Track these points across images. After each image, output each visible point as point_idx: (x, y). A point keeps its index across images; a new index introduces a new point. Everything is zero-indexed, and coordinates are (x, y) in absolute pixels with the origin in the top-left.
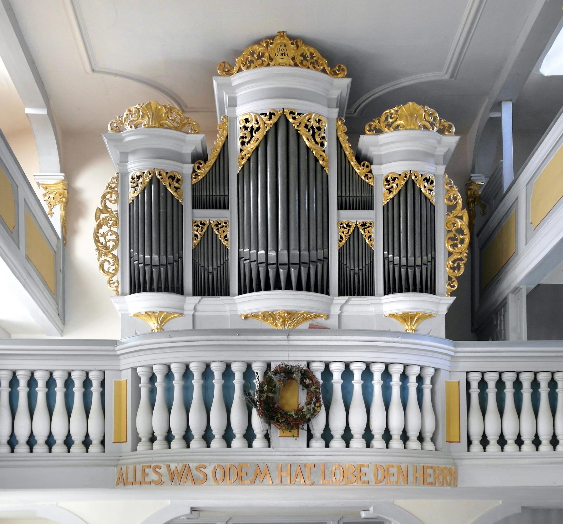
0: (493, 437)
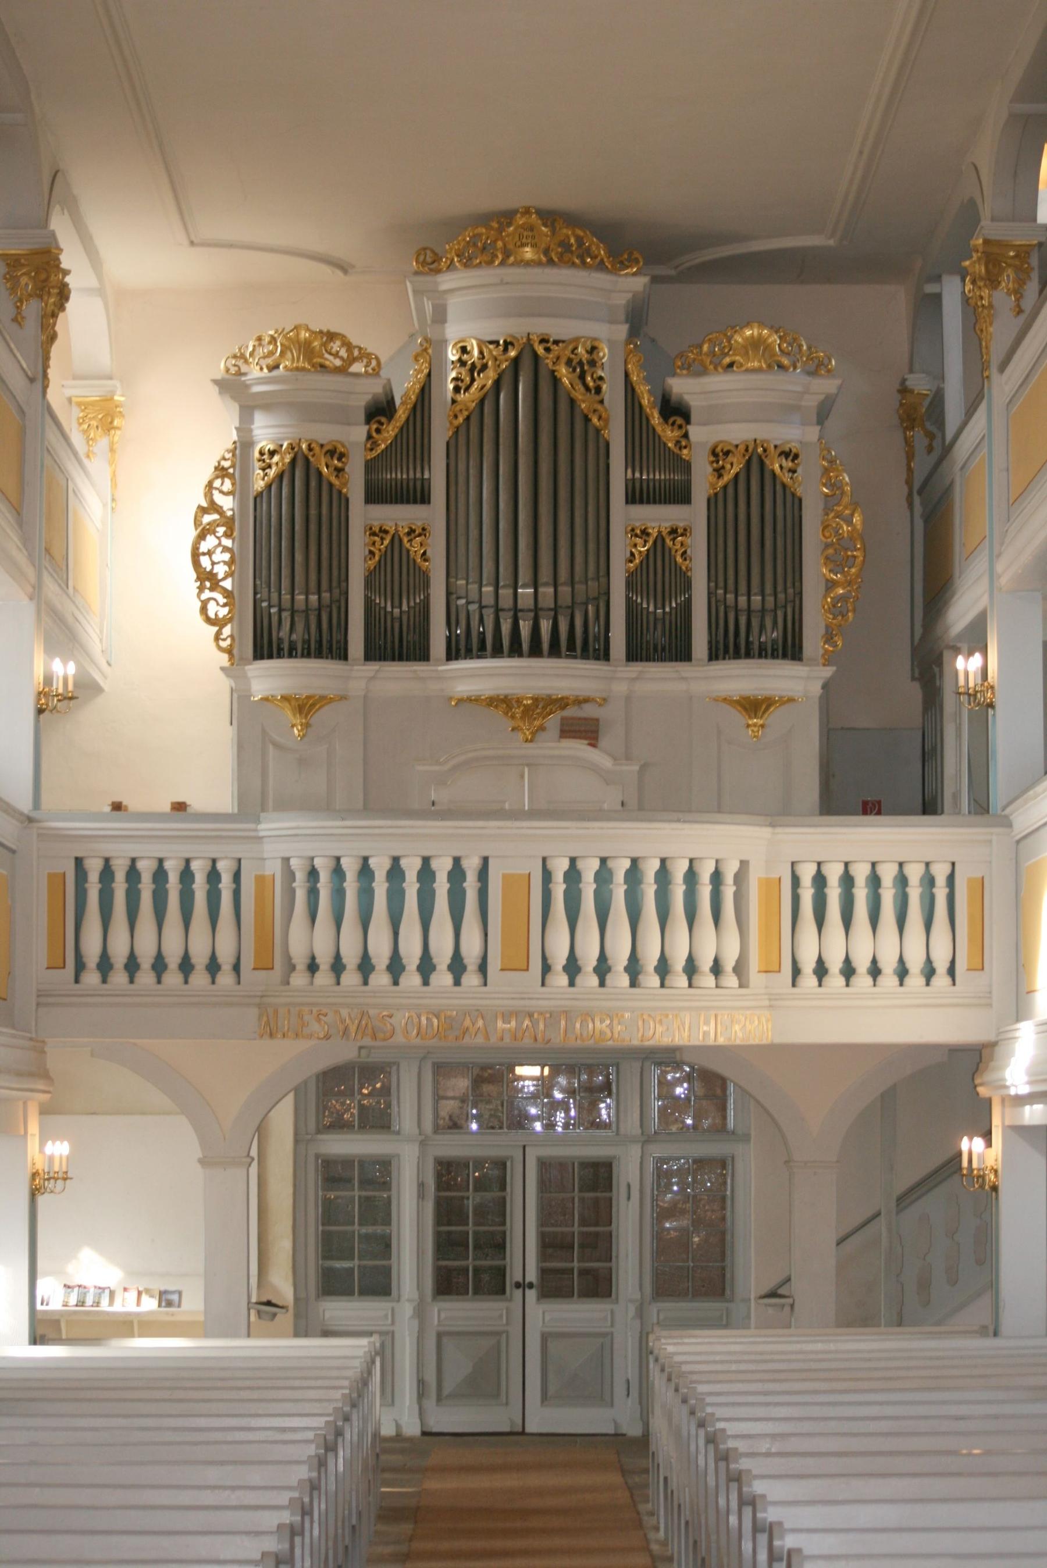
0: (835, 964)
